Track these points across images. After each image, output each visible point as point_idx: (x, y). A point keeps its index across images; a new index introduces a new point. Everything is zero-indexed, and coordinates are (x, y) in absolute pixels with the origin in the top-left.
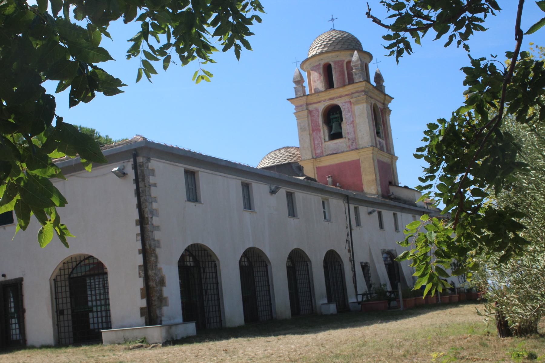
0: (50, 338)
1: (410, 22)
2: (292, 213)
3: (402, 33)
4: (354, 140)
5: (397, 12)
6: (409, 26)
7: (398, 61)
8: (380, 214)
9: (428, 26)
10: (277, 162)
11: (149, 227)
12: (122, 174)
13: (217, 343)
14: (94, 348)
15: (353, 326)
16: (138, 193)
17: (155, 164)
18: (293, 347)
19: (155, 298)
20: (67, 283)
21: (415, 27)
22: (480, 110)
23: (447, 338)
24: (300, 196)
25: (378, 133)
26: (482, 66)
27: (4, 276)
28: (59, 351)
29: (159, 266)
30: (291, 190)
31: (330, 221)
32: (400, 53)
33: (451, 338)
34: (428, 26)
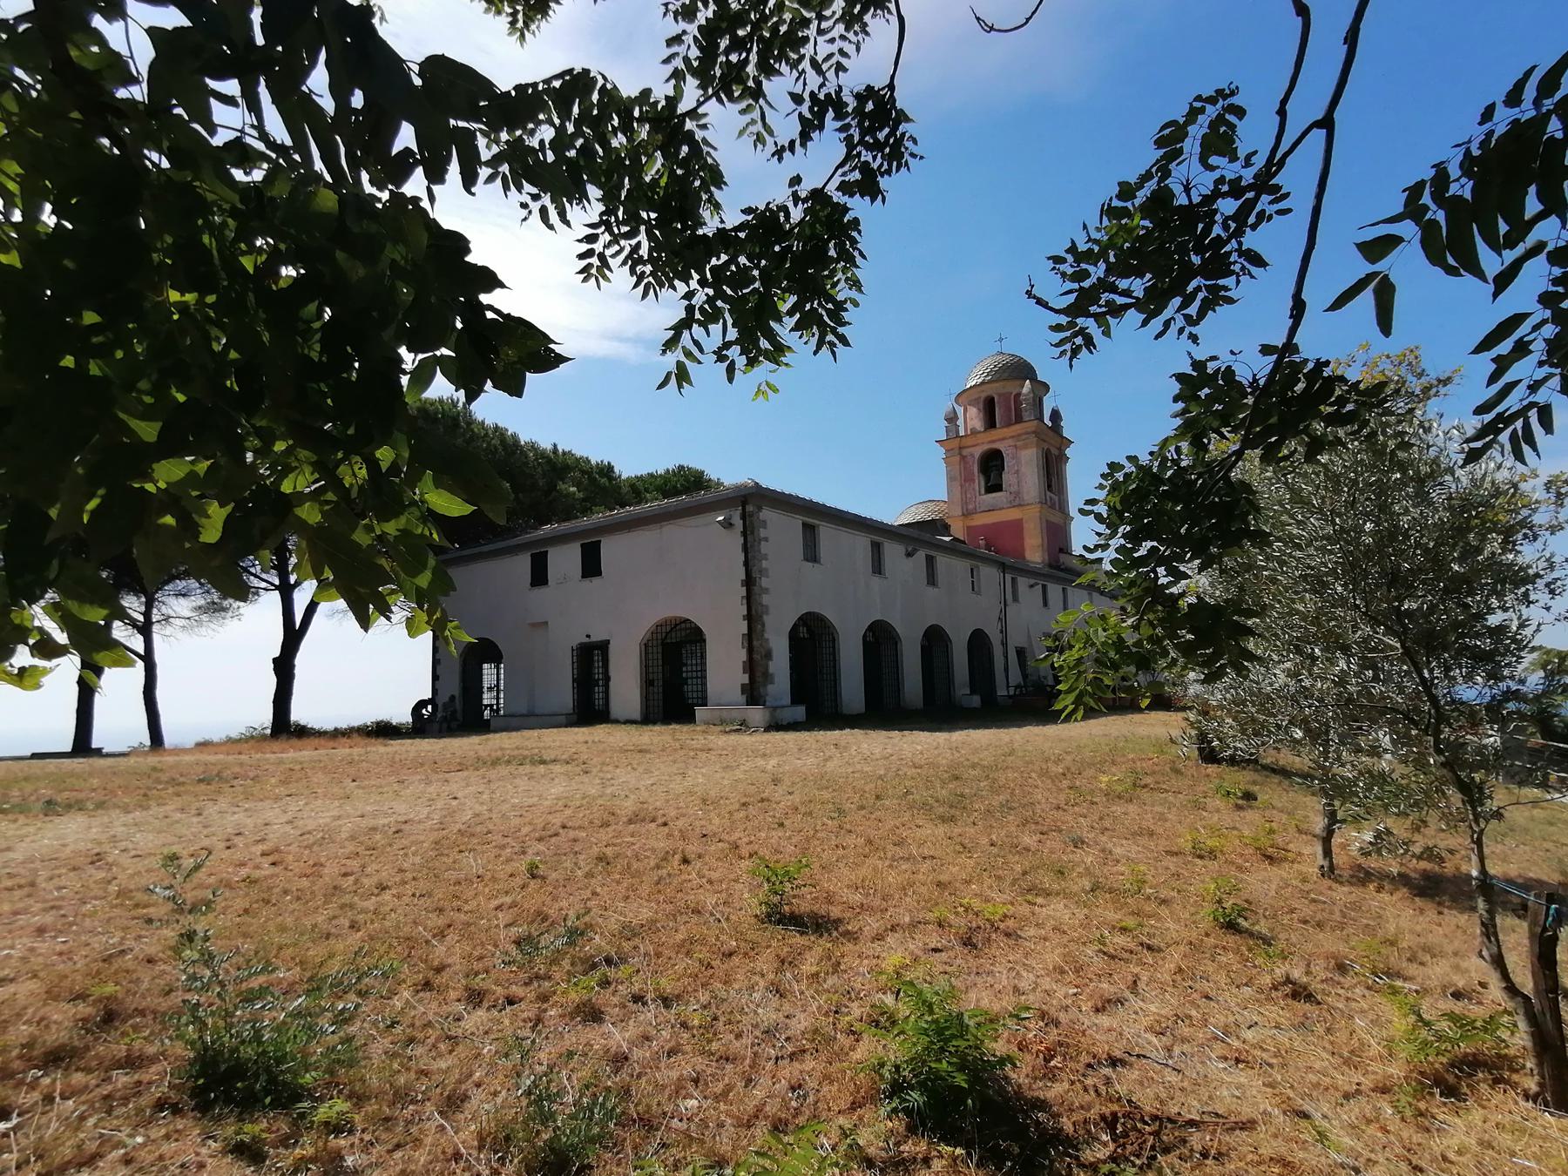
0: (637, 715)
1: (1096, 302)
2: (932, 580)
3: (1080, 321)
4: (1018, 494)
5: (1076, 286)
6: (1093, 309)
7: (1071, 366)
8: (1044, 587)
9: (1126, 307)
10: (918, 518)
11: (756, 589)
12: (727, 524)
13: (829, 733)
14: (685, 728)
15: (998, 727)
16: (745, 549)
17: (767, 514)
18: (919, 748)
19: (758, 674)
20: (660, 650)
21: (1104, 309)
22: (1199, 446)
23: (1124, 756)
24: (942, 561)
25: (1049, 486)
26: (1210, 371)
27: (588, 636)
28: (645, 728)
29: (766, 636)
30: (932, 553)
31: (979, 593)
32: (1075, 352)
33: (1131, 756)
34: (1126, 307)
